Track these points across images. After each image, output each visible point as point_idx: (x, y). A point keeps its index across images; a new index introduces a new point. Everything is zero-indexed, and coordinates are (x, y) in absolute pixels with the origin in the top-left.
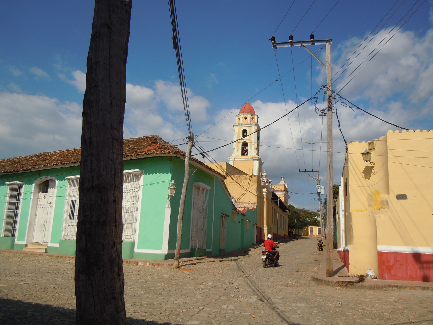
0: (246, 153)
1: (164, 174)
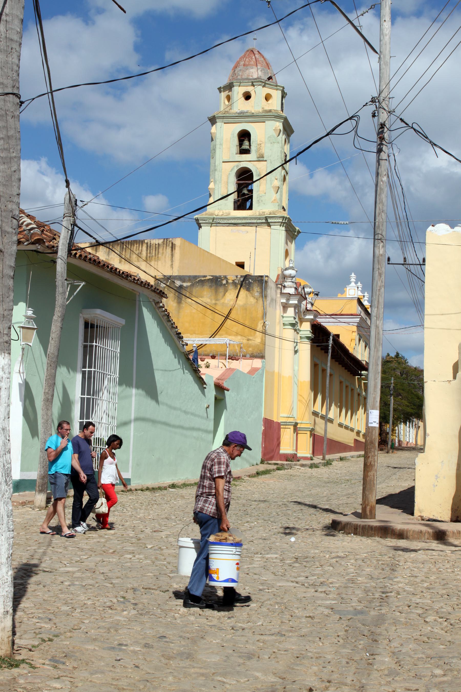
0: (248, 204)
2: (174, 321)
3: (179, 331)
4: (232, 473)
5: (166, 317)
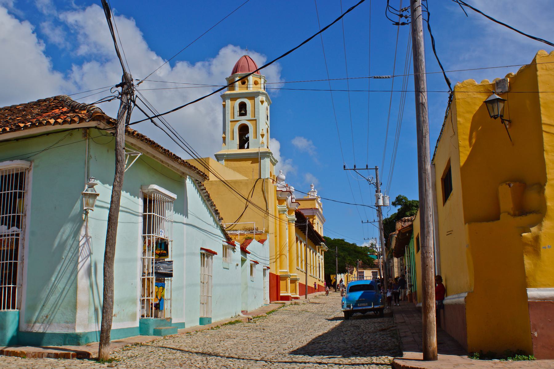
0: (246, 145)
1: (127, 193)
2: (213, 201)
3: (216, 209)
4: (168, 282)
5: (207, 197)
